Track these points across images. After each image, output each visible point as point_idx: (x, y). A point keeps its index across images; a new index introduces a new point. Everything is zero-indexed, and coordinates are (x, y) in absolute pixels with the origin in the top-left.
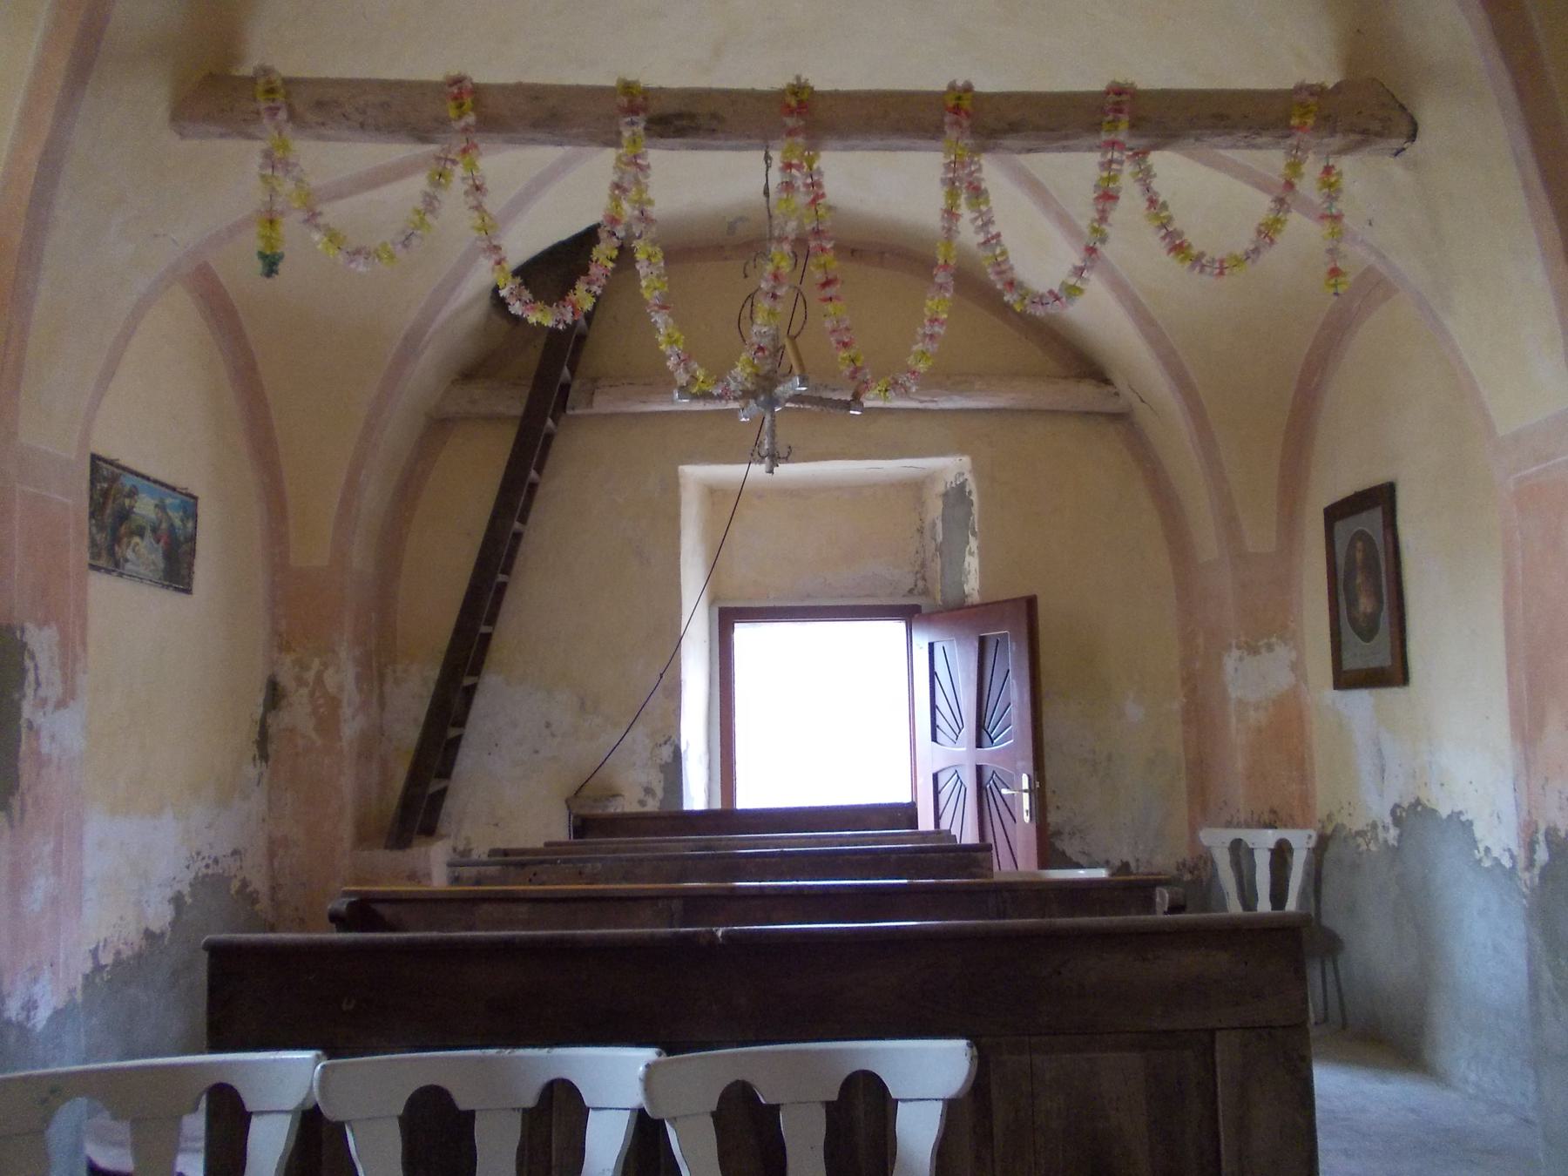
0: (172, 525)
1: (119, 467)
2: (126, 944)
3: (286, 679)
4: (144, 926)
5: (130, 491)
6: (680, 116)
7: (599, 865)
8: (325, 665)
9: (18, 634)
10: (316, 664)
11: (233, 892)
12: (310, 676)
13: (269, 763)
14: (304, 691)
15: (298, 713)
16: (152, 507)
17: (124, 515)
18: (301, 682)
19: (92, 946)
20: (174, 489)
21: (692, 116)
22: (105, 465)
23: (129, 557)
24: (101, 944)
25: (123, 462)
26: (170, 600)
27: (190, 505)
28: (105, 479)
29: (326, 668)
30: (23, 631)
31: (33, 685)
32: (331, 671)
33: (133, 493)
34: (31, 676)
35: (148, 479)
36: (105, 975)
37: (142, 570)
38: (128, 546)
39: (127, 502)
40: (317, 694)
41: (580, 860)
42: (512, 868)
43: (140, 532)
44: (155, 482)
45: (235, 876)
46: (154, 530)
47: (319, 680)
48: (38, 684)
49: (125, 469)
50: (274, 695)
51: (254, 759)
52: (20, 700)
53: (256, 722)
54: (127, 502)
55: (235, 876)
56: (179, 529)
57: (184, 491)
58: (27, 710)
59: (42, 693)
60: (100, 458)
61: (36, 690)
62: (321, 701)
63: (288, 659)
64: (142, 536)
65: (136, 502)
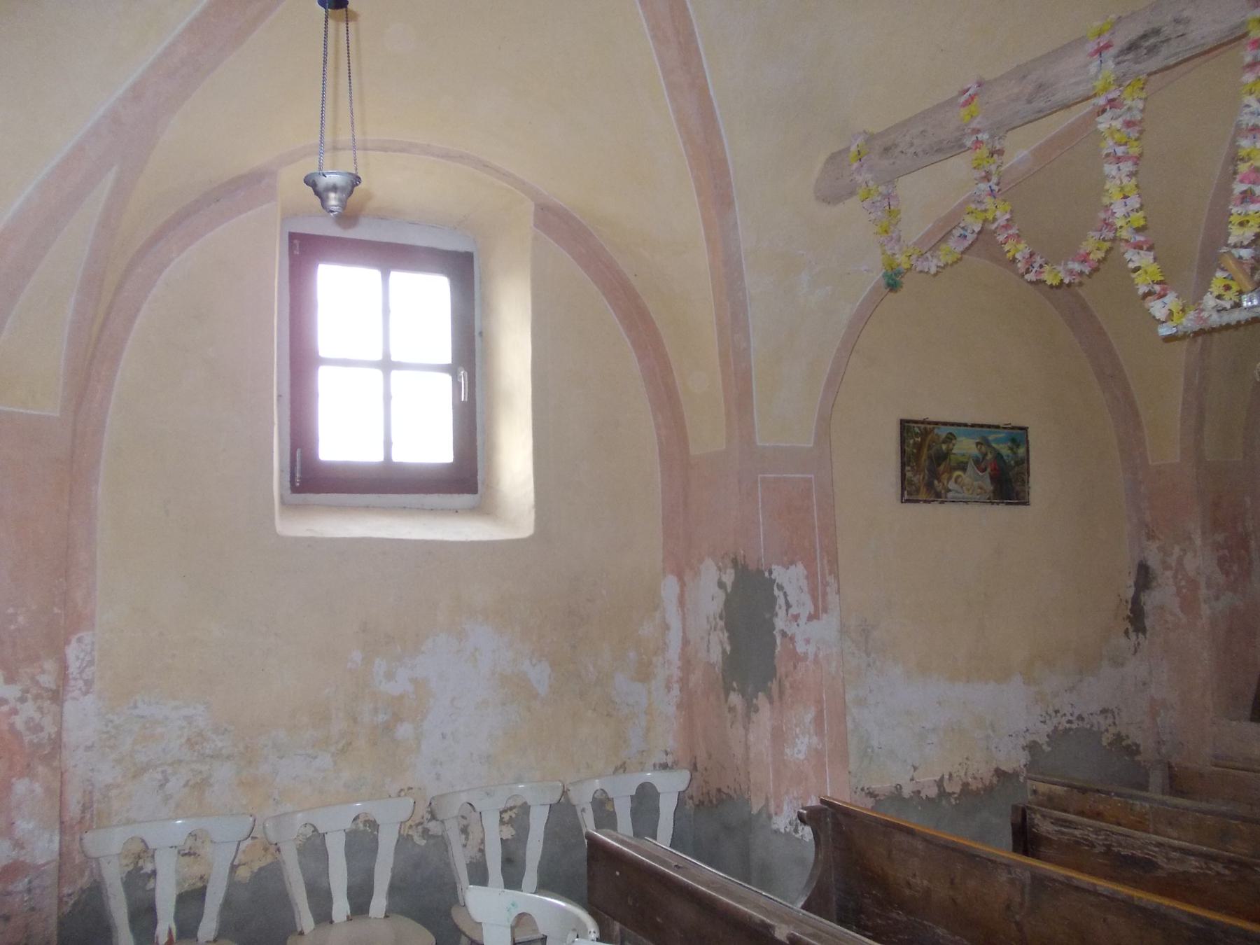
0: (999, 456)
1: (929, 423)
2: (975, 778)
3: (1154, 562)
4: (995, 766)
5: (947, 437)
6: (1145, 37)
7: (1147, 805)
8: (1184, 551)
9: (767, 574)
10: (1177, 550)
11: (1104, 743)
12: (1172, 561)
13: (1148, 635)
14: (1169, 573)
15: (1162, 596)
16: (974, 446)
17: (942, 457)
18: (1167, 567)
19: (937, 778)
20: (998, 427)
21: (1156, 32)
22: (915, 425)
23: (950, 488)
24: (947, 777)
25: (932, 418)
26: (1003, 513)
27: (1018, 436)
28: (917, 435)
29: (1185, 554)
30: (771, 573)
31: (784, 608)
32: (1189, 555)
33: (951, 438)
34: (781, 601)
35: (966, 425)
36: (953, 800)
37: (967, 495)
38: (949, 479)
39: (944, 447)
40: (1180, 577)
41: (1131, 797)
42: (1075, 791)
43: (963, 467)
44: (973, 426)
45: (1107, 730)
46: (977, 462)
47: (1180, 561)
48: (788, 606)
49: (937, 423)
50: (1144, 577)
51: (1126, 632)
52: (771, 619)
53: (1127, 602)
54: (944, 447)
55: (1107, 730)
56: (1008, 456)
57: (1010, 426)
58: (780, 623)
59: (793, 611)
60: (908, 421)
61: (787, 610)
62: (1183, 583)
63: (1154, 545)
64: (964, 469)
65: (954, 445)
